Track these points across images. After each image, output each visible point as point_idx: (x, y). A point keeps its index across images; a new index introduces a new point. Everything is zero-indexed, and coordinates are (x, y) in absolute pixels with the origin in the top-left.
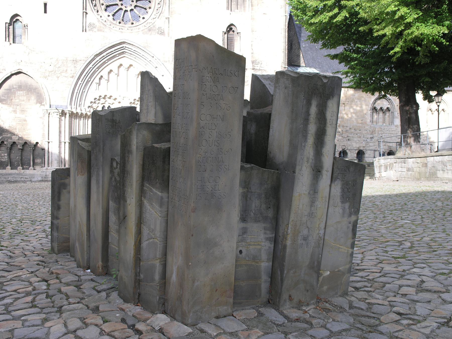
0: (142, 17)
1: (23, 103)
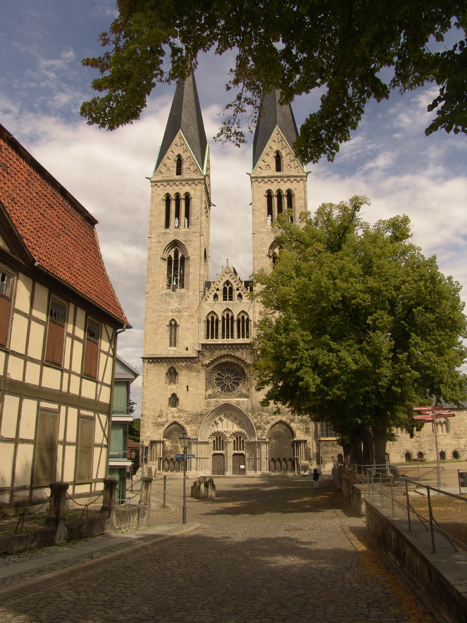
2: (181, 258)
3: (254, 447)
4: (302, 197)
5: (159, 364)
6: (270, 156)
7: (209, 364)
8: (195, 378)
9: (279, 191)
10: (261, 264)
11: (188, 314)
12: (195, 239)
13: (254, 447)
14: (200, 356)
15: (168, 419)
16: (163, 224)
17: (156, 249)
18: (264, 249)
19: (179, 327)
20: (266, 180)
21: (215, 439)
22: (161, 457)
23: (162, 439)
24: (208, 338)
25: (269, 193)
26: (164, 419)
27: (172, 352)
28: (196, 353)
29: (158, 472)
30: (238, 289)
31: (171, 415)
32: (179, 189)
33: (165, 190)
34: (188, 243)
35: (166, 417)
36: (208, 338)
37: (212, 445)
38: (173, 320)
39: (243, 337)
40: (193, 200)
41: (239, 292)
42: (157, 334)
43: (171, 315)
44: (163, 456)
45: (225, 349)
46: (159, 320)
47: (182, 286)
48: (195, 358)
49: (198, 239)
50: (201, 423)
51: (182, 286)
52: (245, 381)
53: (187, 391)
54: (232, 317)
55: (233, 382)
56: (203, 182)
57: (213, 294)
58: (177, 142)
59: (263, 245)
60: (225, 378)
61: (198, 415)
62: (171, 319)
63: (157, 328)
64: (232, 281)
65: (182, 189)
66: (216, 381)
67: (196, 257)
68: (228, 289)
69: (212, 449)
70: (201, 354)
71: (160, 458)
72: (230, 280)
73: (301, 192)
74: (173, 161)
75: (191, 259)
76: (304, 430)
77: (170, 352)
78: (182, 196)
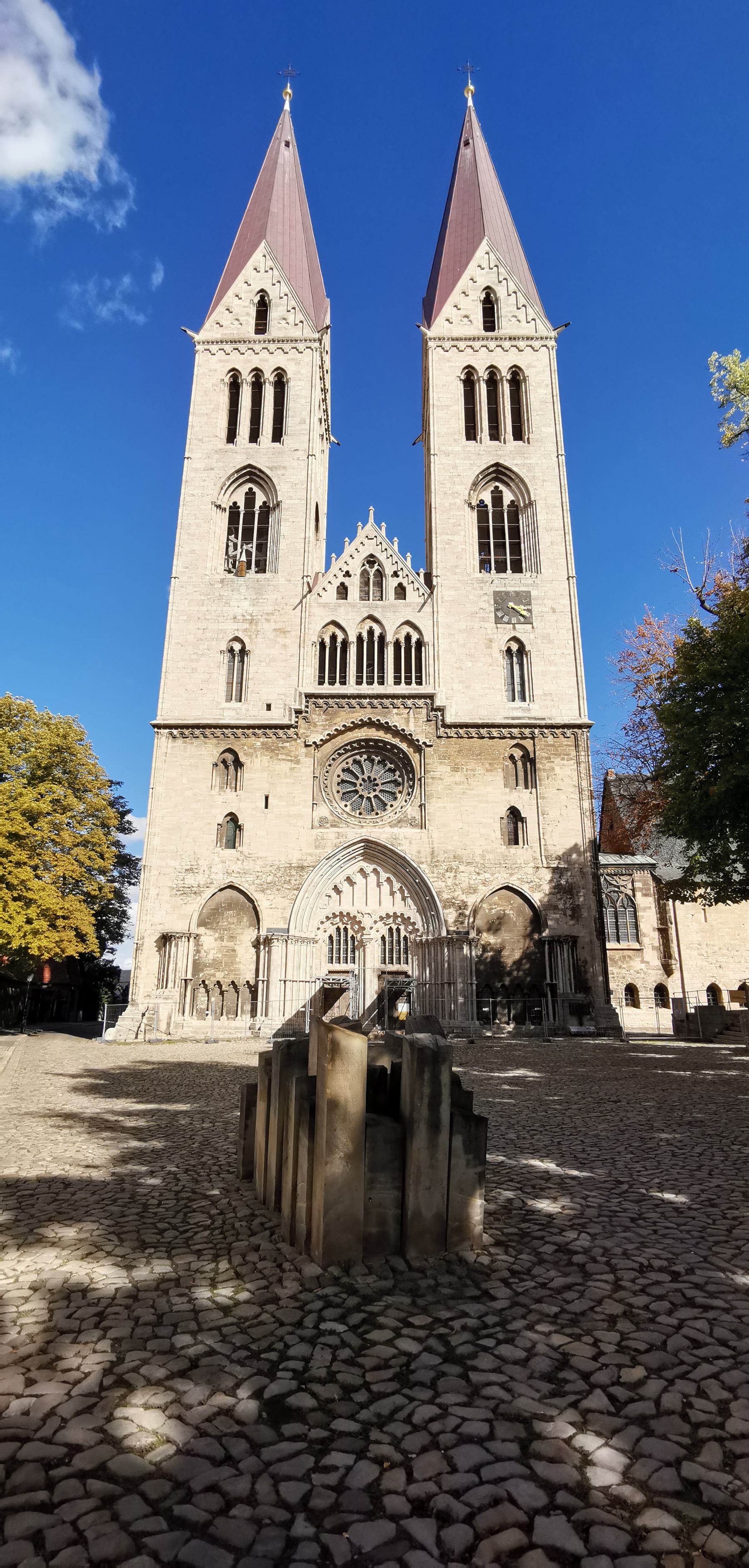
0: (389, 804)
1: (233, 926)
2: (260, 507)
3: (436, 955)
4: (546, 382)
5: (196, 742)
6: (471, 297)
7: (324, 742)
8: (286, 777)
9: (493, 371)
10: (451, 521)
11: (273, 626)
12: (295, 463)
13: (436, 955)
14: (301, 722)
15: (213, 876)
16: (223, 434)
17: (202, 484)
18: (458, 488)
19: (251, 656)
20: (462, 345)
21: (332, 931)
22: (189, 976)
23: (194, 930)
24: (321, 683)
25: (470, 371)
26: (201, 879)
27: (232, 714)
28: (290, 715)
29: (177, 1018)
30: (396, 574)
31: (220, 866)
32: (261, 360)
33: (228, 361)
34: (279, 472)
35: (207, 872)
36: (321, 683)
37: (326, 949)
38: (237, 639)
39: (409, 683)
40: (291, 384)
41: (400, 580)
42: (194, 670)
43: (232, 629)
44: (193, 975)
45: (362, 707)
46: (201, 640)
47: (261, 568)
48: (288, 727)
49: (303, 464)
50: (298, 889)
51: (261, 568)
52: (412, 787)
53: (266, 807)
54: (382, 638)
55: (381, 791)
56: (317, 344)
57: (337, 583)
58: (257, 264)
59: (457, 480)
60: (360, 781)
61: (291, 867)
62: (231, 637)
63: (195, 657)
64: (382, 557)
65: (266, 360)
66: (339, 788)
67: (297, 501)
68: (372, 574)
69: (325, 959)
70: (305, 718)
71: (186, 980)
72: (377, 555)
73: (544, 371)
74: (247, 303)
75: (283, 505)
76: (569, 912)
77: (226, 713)
78: (269, 377)
